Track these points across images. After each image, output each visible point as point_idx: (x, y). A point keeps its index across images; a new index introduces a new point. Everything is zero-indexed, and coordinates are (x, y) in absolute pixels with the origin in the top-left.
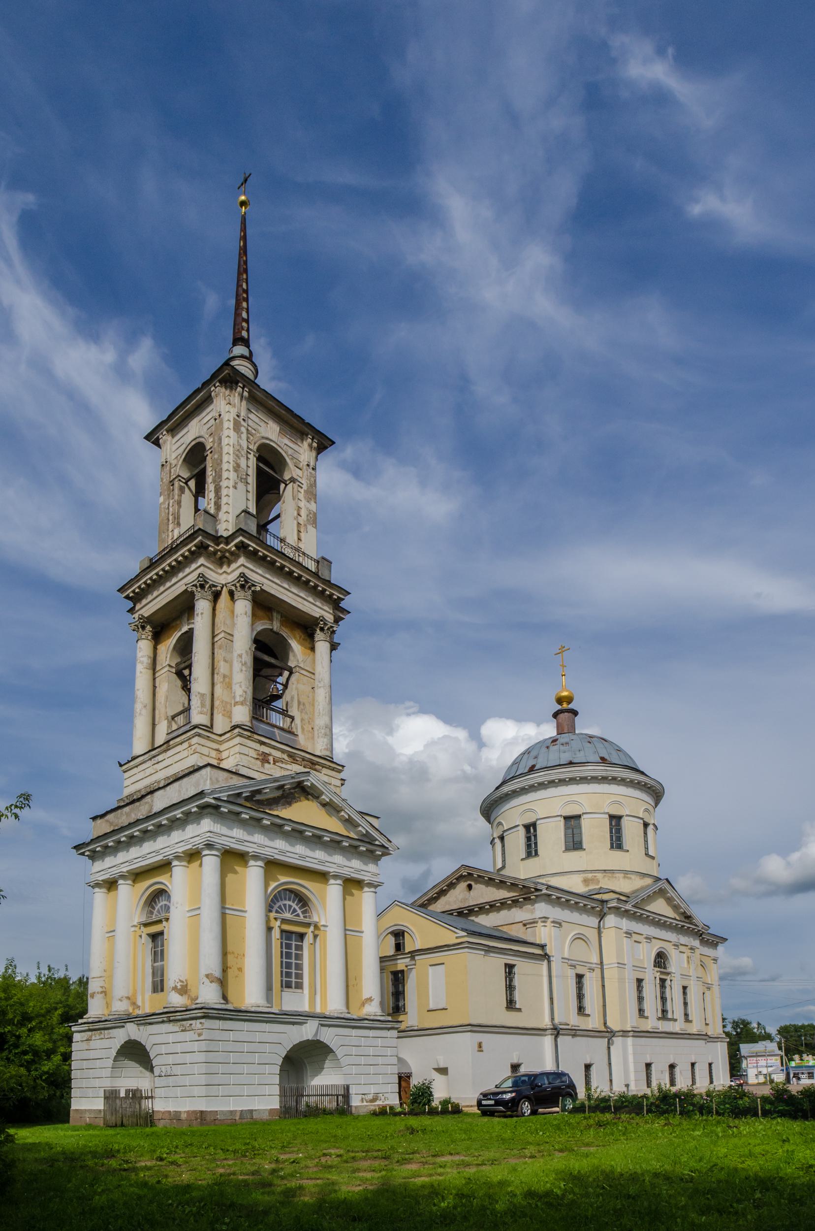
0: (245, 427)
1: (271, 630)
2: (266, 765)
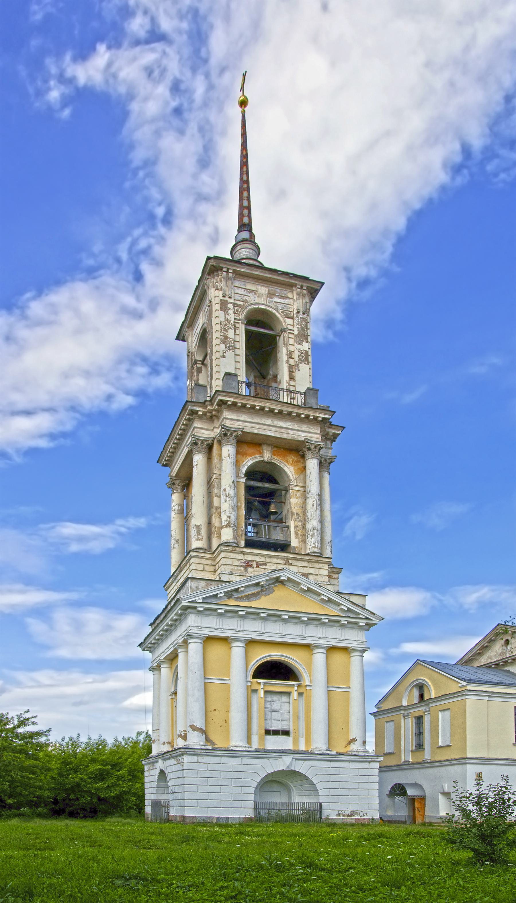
0: (231, 303)
1: (263, 461)
2: (250, 570)
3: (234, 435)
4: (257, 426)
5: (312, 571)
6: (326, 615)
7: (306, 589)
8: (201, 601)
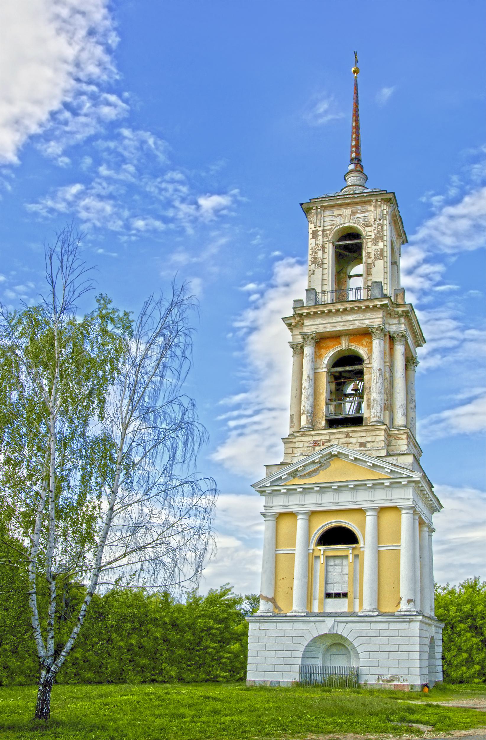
3: (310, 337)
4: (329, 325)
5: (369, 439)
6: (369, 480)
7: (353, 459)
8: (269, 485)
